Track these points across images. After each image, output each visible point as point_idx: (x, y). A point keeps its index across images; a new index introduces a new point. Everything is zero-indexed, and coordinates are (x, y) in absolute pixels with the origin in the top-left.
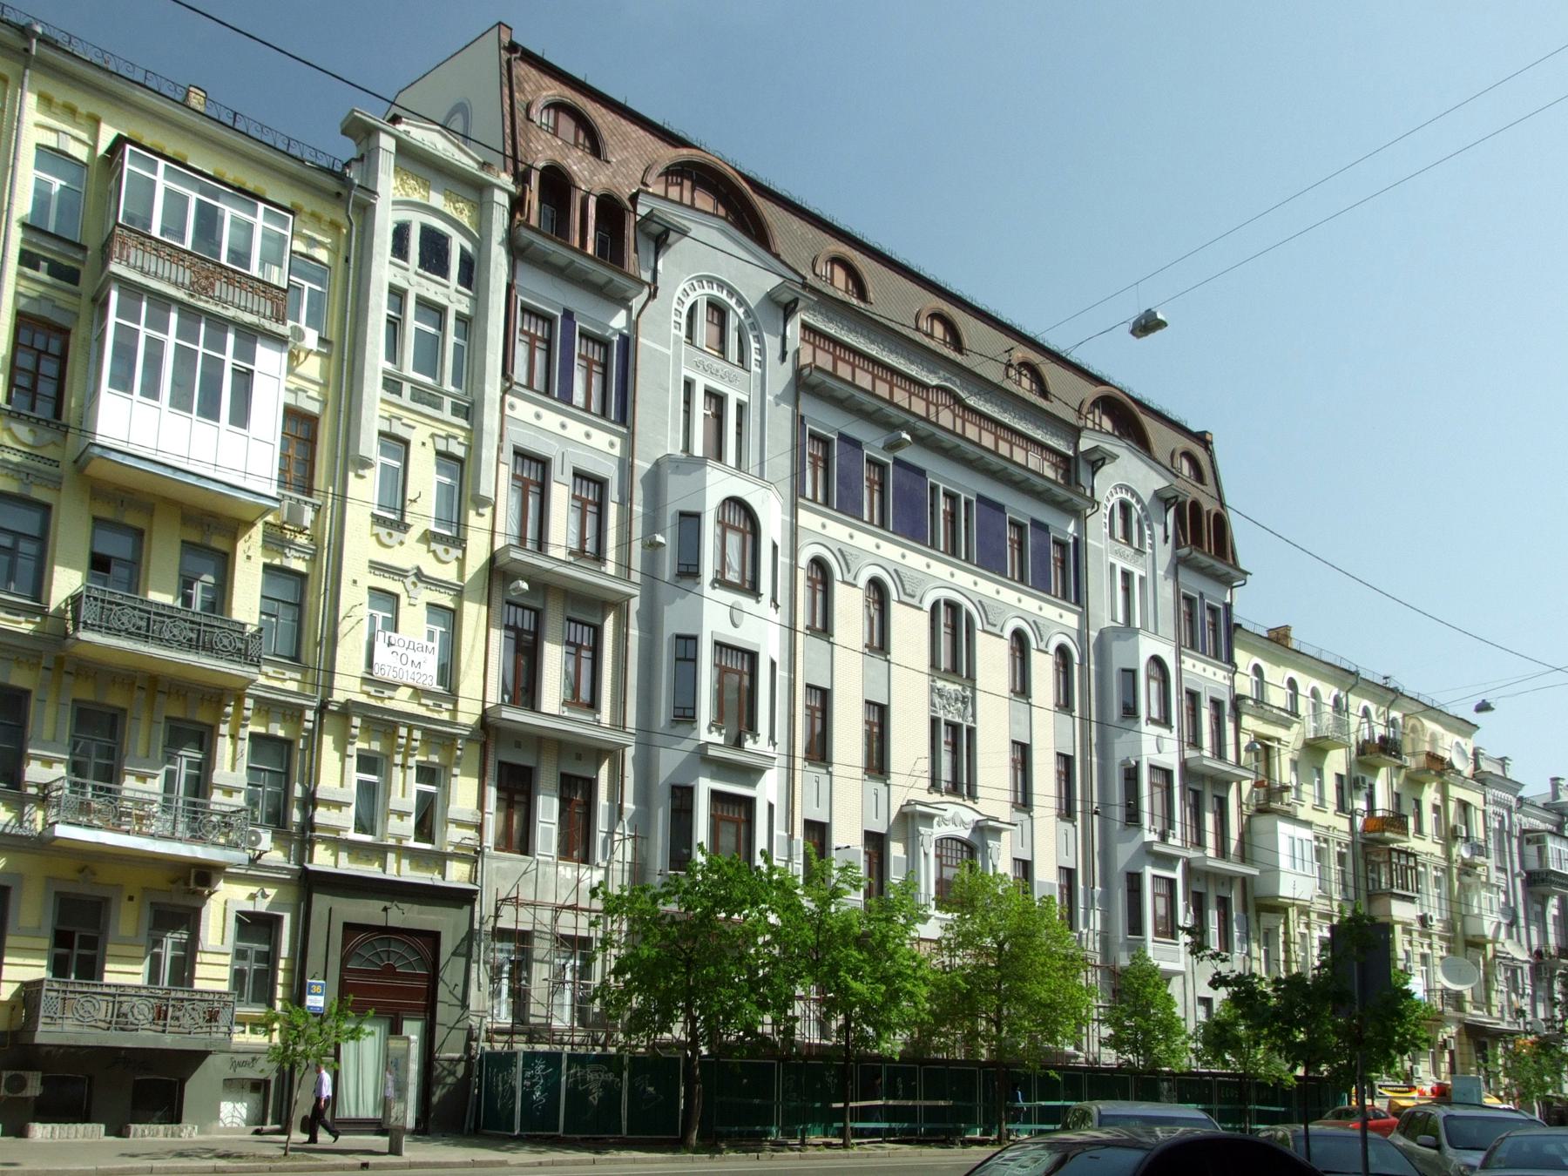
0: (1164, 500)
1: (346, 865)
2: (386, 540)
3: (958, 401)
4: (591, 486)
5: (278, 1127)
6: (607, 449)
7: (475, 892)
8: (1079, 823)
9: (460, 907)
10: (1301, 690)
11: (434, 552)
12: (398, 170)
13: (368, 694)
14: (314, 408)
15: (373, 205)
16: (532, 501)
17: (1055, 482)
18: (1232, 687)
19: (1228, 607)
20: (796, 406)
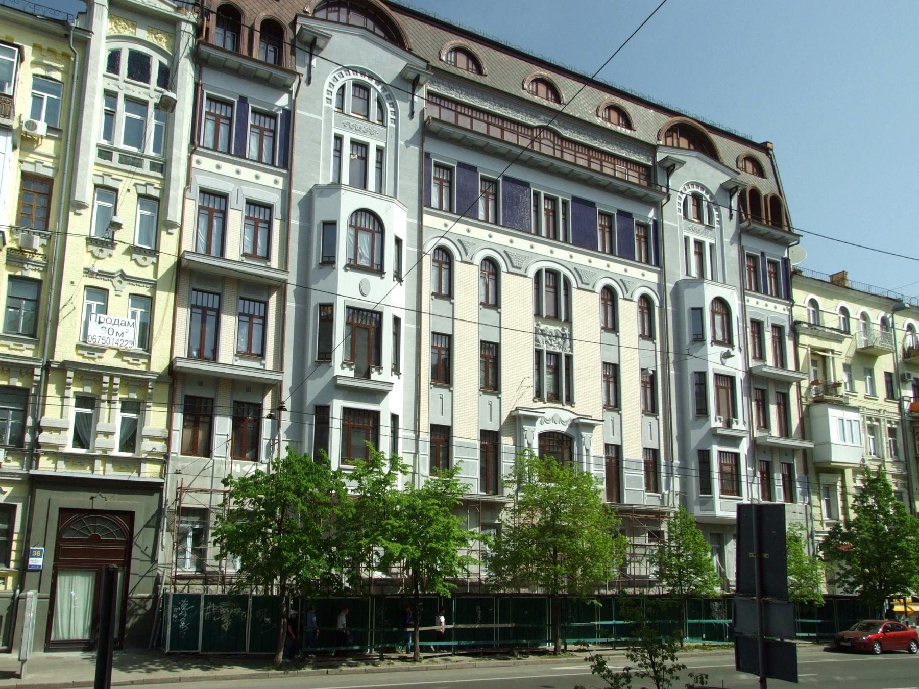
0: (728, 190)
1: (63, 470)
2: (142, 262)
3: (556, 134)
4: (259, 211)
5: (5, 647)
6: (272, 184)
7: (162, 484)
8: (661, 417)
9: (152, 494)
10: (851, 314)
11: (135, 260)
12: (111, 16)
13: (83, 355)
14: (49, 173)
15: (90, 40)
16: (444, 273)
17: (639, 185)
18: (791, 315)
19: (786, 261)
20: (422, 146)
